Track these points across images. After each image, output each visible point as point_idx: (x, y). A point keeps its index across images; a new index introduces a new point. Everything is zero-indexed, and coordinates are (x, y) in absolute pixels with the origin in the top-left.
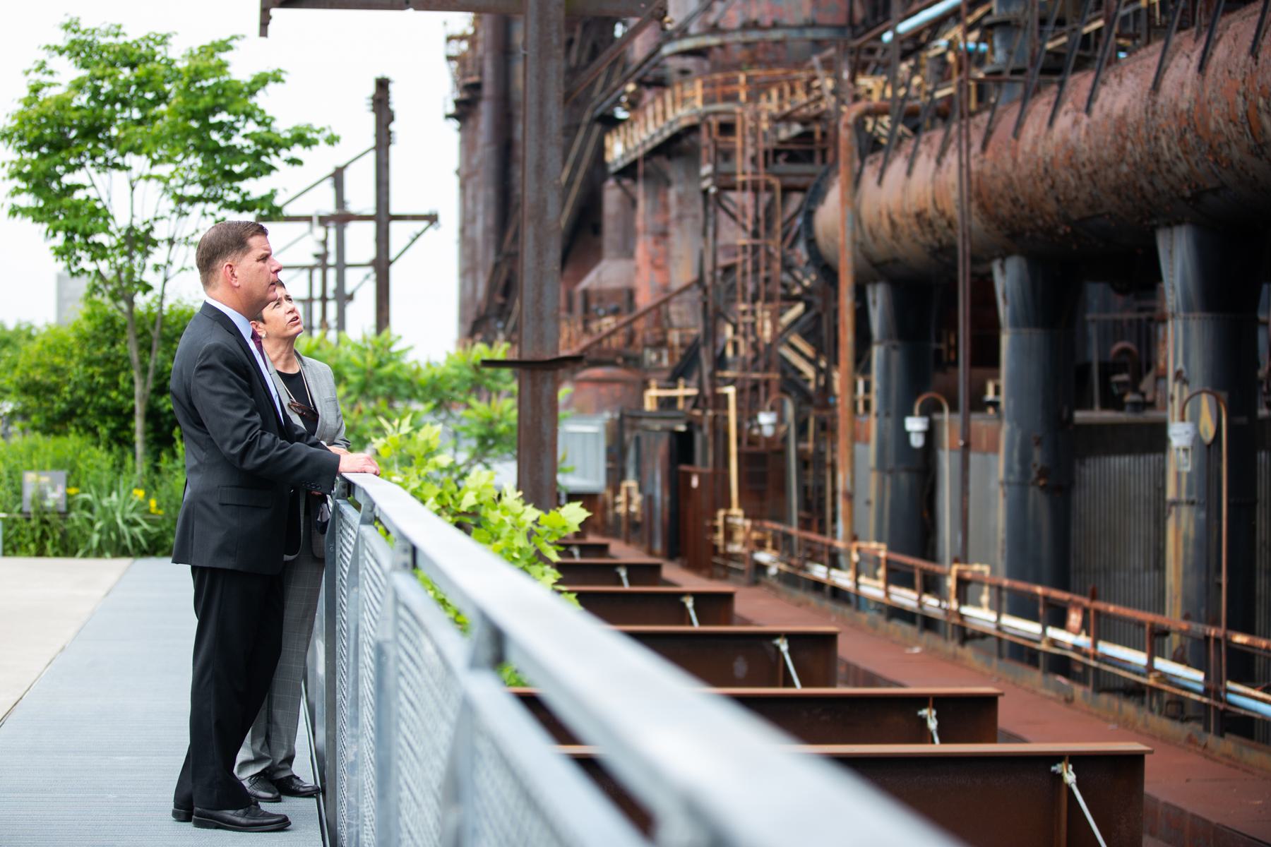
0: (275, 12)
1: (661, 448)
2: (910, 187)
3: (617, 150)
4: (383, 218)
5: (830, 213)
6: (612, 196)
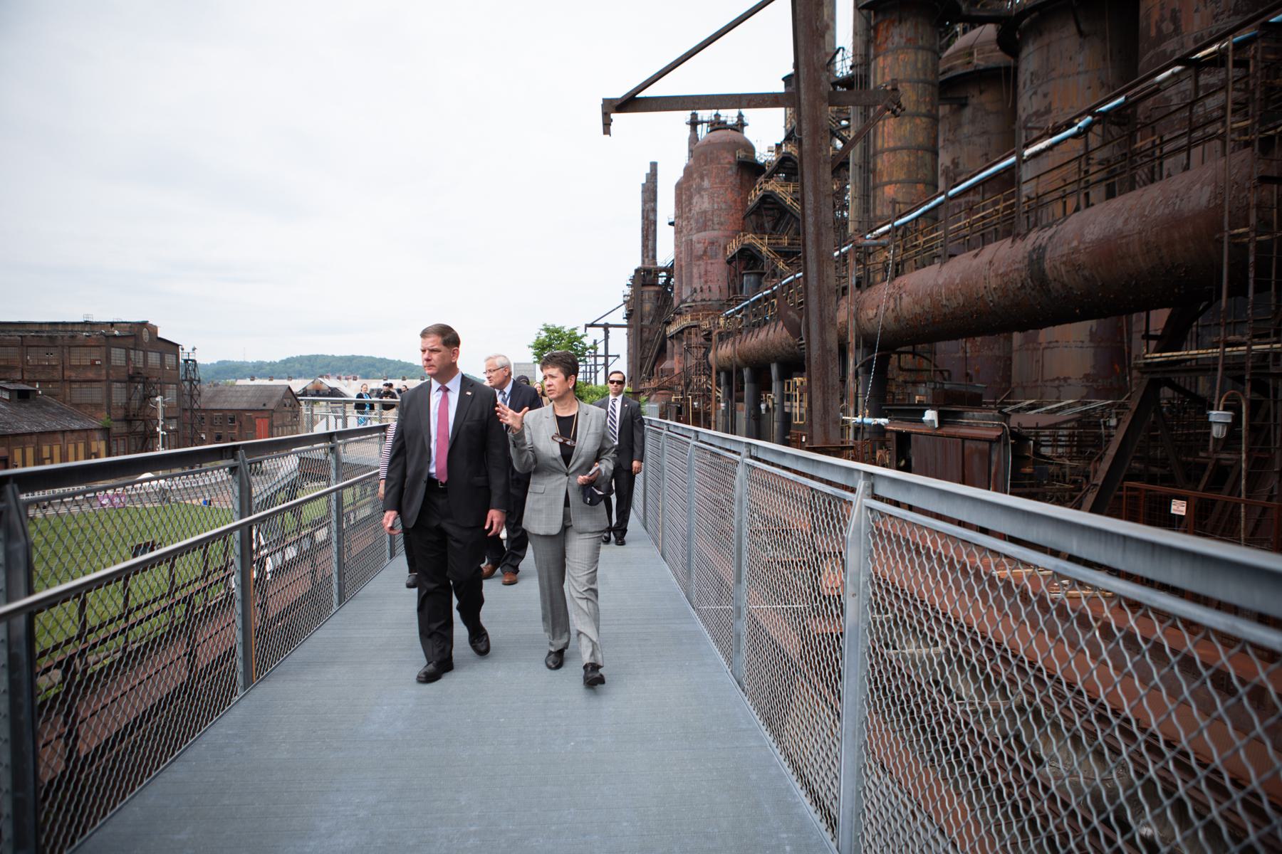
0: (613, 116)
1: (675, 411)
2: (725, 351)
3: (672, 330)
4: (607, 356)
5: (711, 355)
6: (669, 342)
